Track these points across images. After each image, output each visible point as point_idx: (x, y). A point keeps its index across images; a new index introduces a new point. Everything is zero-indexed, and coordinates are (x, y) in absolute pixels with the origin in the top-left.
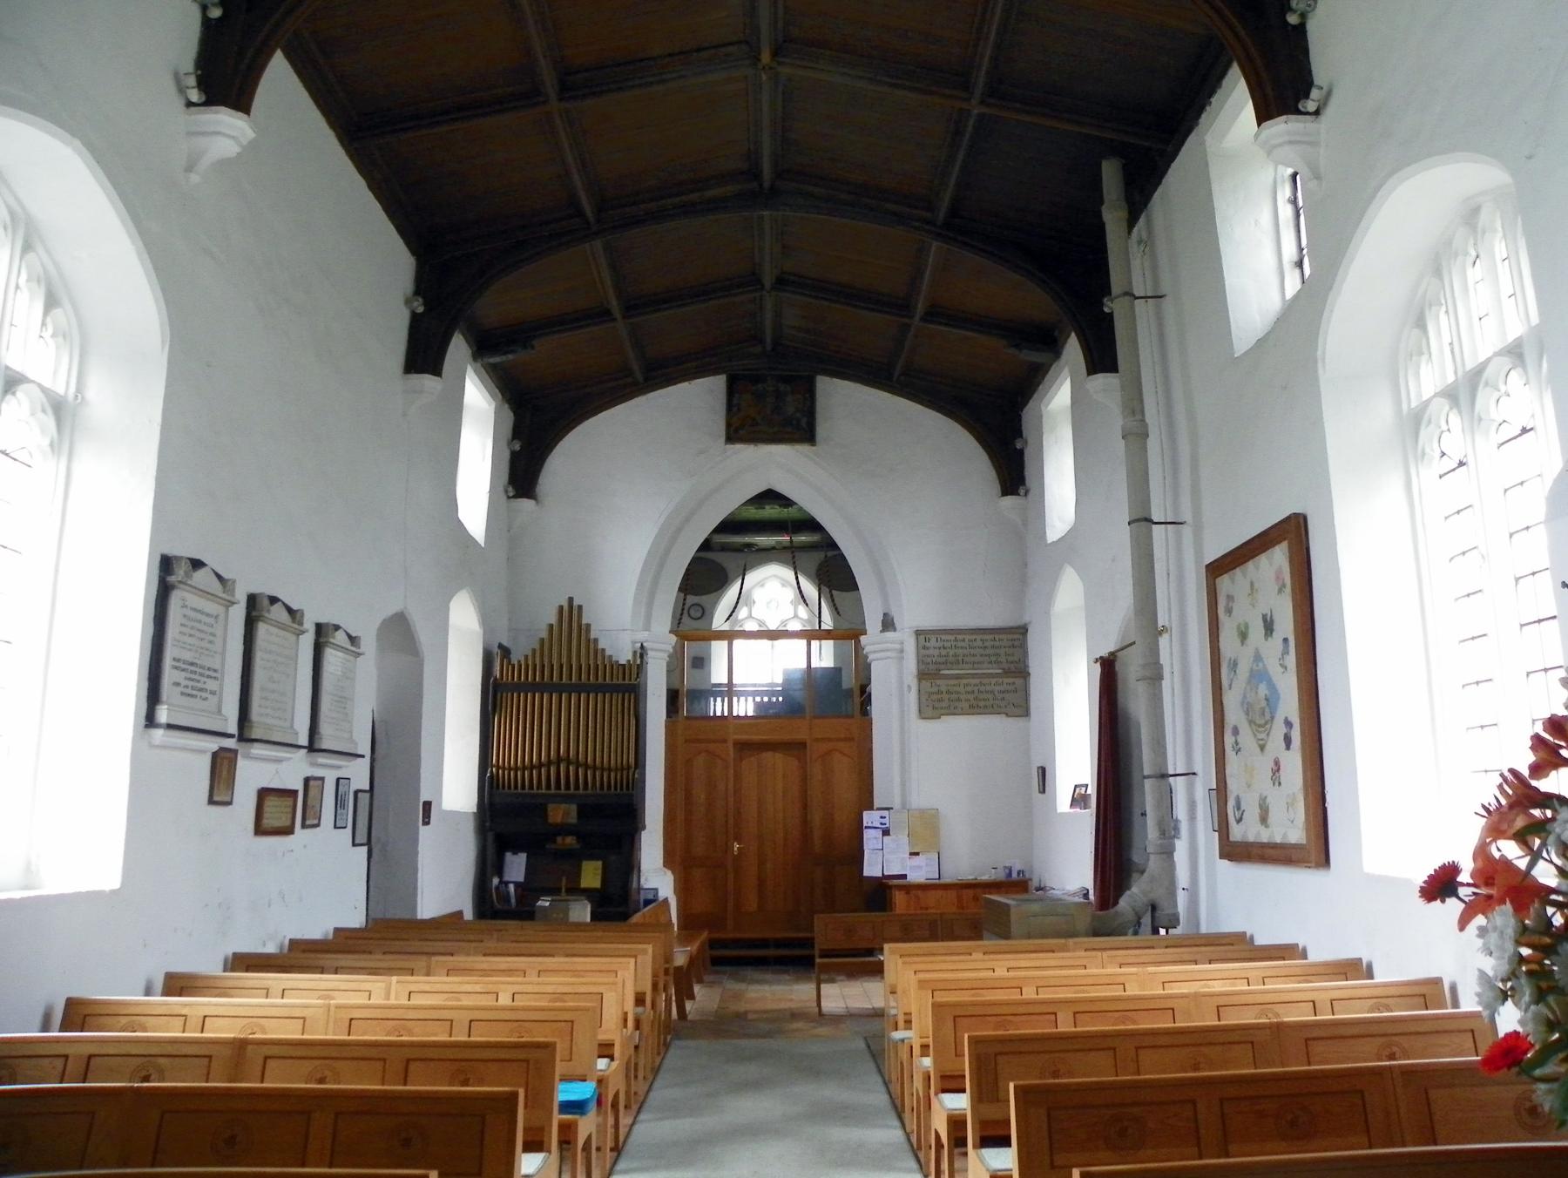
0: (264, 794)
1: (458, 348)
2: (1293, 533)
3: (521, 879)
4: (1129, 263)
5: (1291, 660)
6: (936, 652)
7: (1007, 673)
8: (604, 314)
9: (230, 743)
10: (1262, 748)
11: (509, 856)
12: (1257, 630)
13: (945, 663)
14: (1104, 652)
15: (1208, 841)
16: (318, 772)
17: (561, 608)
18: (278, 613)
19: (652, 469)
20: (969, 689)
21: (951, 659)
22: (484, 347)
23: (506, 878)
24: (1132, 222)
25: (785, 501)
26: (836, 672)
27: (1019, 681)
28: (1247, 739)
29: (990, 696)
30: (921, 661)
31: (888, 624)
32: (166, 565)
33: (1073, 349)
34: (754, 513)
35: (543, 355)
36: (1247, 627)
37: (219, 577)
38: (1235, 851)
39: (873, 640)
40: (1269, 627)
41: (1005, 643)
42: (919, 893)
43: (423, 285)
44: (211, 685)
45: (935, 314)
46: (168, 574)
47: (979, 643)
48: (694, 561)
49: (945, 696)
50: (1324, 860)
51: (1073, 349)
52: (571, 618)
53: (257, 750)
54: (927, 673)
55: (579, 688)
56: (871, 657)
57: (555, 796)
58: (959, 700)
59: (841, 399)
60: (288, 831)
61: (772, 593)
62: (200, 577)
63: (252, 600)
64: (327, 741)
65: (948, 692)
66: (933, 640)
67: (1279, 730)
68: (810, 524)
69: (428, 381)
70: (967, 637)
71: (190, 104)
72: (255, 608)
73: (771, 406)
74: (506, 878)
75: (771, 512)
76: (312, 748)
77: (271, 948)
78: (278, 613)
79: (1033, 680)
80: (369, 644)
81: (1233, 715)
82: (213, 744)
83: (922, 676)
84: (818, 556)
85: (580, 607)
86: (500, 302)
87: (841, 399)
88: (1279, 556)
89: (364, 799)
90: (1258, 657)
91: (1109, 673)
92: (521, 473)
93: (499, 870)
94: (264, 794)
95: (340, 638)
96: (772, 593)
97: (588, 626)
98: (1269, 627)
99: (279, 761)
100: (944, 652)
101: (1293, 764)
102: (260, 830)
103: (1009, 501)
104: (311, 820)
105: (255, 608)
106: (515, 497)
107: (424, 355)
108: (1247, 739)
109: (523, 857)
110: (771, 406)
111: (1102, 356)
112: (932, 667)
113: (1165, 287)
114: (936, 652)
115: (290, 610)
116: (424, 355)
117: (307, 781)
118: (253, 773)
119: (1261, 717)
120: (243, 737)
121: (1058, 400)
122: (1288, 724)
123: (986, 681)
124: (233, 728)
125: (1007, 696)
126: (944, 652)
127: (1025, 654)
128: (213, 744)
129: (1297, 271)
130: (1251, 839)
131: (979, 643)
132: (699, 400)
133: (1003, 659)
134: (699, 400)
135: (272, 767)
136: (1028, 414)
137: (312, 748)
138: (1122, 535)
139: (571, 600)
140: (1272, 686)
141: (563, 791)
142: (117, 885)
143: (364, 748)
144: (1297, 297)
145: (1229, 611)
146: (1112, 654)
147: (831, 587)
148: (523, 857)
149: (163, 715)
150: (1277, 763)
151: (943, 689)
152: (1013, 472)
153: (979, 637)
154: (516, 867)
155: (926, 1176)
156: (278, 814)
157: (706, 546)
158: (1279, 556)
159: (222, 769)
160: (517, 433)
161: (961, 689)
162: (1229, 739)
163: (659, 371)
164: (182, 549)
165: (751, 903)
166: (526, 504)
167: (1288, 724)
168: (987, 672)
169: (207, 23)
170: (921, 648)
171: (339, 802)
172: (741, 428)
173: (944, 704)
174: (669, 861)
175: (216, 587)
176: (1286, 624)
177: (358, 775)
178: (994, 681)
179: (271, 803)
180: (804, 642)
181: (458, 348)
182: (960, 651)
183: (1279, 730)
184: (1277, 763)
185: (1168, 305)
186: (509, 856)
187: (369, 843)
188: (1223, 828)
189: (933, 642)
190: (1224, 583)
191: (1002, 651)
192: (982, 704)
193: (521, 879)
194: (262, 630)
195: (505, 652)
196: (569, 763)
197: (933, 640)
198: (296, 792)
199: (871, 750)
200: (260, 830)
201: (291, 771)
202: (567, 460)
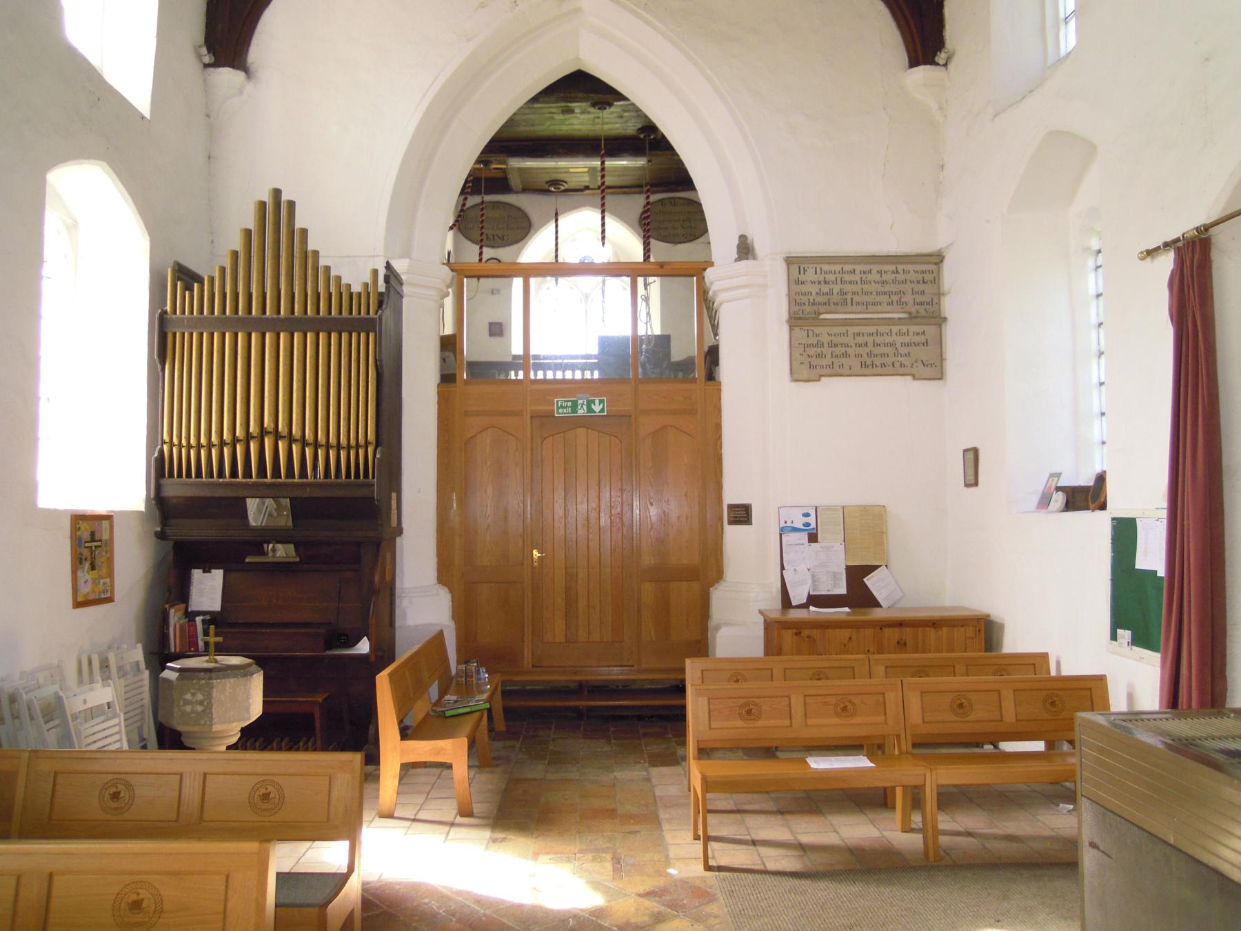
3: (216, 606)
6: (814, 289)
7: (913, 318)
11: (197, 574)
13: (828, 303)
14: (1182, 225)
17: (262, 205)
20: (860, 340)
21: (835, 298)
23: (194, 607)
26: (663, 342)
27: (931, 330)
29: (889, 350)
30: (794, 300)
31: (745, 250)
39: (724, 274)
41: (913, 276)
42: (816, 633)
47: (875, 276)
49: (826, 350)
52: (277, 214)
54: (801, 317)
55: (293, 325)
56: (718, 300)
57: (255, 485)
58: (846, 355)
61: (586, 232)
65: (832, 345)
66: (811, 271)
70: (858, 268)
71: (206, 66)
74: (194, 607)
75: (582, 120)
79: (949, 331)
83: (795, 320)
85: (291, 205)
93: (181, 592)
96: (586, 232)
97: (304, 232)
100: (825, 289)
103: (922, 71)
106: (217, 64)
109: (218, 574)
112: (807, 308)
114: (814, 289)
123: (882, 329)
125: (913, 350)
126: (825, 289)
131: (875, 276)
133: (908, 298)
139: (277, 193)
141: (310, 479)
146: (1207, 228)
148: (218, 574)
151: (825, 339)
153: (875, 268)
154: (208, 589)
161: (849, 340)
165: (557, 630)
166: (226, 76)
168: (876, 316)
170: (794, 282)
173: (825, 362)
174: (445, 575)
178: (895, 329)
180: (627, 280)
182: (849, 288)
186: (197, 574)
189: (810, 275)
191: (907, 287)
192: (878, 361)
193: (216, 606)
195: (186, 276)
196: (277, 436)
197: (811, 271)
199: (718, 427)
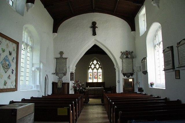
69: (56, 33)
103: (133, 32)
121: (143, 11)
152: (133, 26)
183: (10, 71)
184: (9, 75)
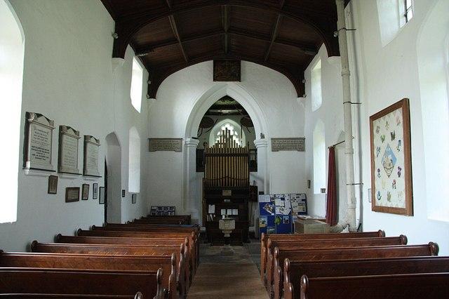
0: (68, 189)
1: (129, 50)
2: (404, 105)
4: (344, 19)
5: (402, 147)
8: (174, 40)
9: (55, 174)
10: (389, 176)
12: (388, 137)
15: (368, 206)
16: (87, 183)
18: (70, 132)
19: (190, 93)
22: (138, 51)
24: (345, 5)
25: (231, 99)
28: (383, 172)
32: (28, 115)
33: (323, 49)
34: (221, 103)
35: (157, 53)
36: (384, 136)
37: (48, 120)
38: (377, 209)
40: (393, 137)
43: (118, 29)
44: (46, 155)
45: (279, 39)
46: (28, 120)
48: (204, 118)
50: (412, 214)
51: (323, 49)
53: (64, 175)
59: (248, 67)
60: (77, 200)
62: (40, 120)
63: (61, 128)
64: (89, 171)
67: (395, 171)
68: (239, 106)
72: (62, 130)
73: (227, 71)
75: (227, 102)
76: (84, 174)
77: (71, 234)
78: (70, 132)
80: (103, 142)
81: (378, 164)
82: (49, 174)
84: (240, 117)
86: (143, 37)
87: (248, 67)
88: (399, 113)
89: (103, 190)
90: (388, 146)
91: (332, 152)
92: (152, 90)
94: (68, 189)
95: (92, 140)
96: (229, 125)
98: (393, 137)
99: (73, 179)
101: (401, 182)
102: (67, 201)
104: (85, 198)
105: (62, 130)
107: (118, 52)
108: (383, 172)
110: (227, 71)
111: (334, 51)
113: (356, 27)
115: (75, 131)
116: (118, 52)
117: (83, 185)
118: (64, 183)
119: (389, 166)
120: (59, 172)
122: (400, 169)
124: (55, 168)
127: (304, 146)
128: (49, 174)
129: (405, 18)
130: (384, 205)
132: (205, 68)
134: (205, 68)
135: (71, 181)
136: (306, 72)
137: (84, 174)
138: (341, 109)
140: (393, 155)
142: (15, 221)
143: (103, 174)
144: (405, 27)
145: (378, 131)
147: (247, 126)
149: (28, 165)
150: (394, 181)
152: (301, 90)
155: (273, 296)
156: (73, 195)
157: (208, 113)
158: (399, 113)
159: (53, 183)
160: (150, 79)
162: (376, 173)
163: (192, 60)
164: (34, 110)
167: (400, 169)
169: (115, 39)
171: (94, 191)
172: (217, 77)
175: (47, 123)
176: (400, 135)
177: (101, 182)
179: (70, 192)
181: (129, 50)
184: (394, 181)
185: (356, 32)
187: (106, 203)
188: (373, 201)
190: (376, 123)
194: (65, 137)
198: (79, 188)
200: (67, 201)
201: (78, 182)
202: (163, 88)
